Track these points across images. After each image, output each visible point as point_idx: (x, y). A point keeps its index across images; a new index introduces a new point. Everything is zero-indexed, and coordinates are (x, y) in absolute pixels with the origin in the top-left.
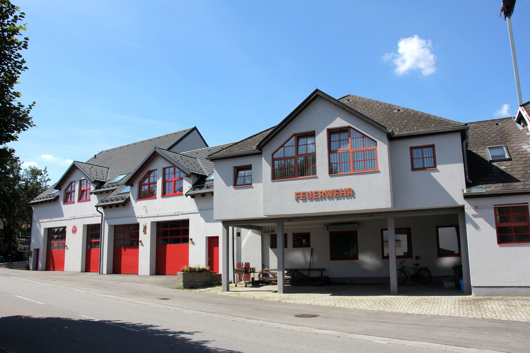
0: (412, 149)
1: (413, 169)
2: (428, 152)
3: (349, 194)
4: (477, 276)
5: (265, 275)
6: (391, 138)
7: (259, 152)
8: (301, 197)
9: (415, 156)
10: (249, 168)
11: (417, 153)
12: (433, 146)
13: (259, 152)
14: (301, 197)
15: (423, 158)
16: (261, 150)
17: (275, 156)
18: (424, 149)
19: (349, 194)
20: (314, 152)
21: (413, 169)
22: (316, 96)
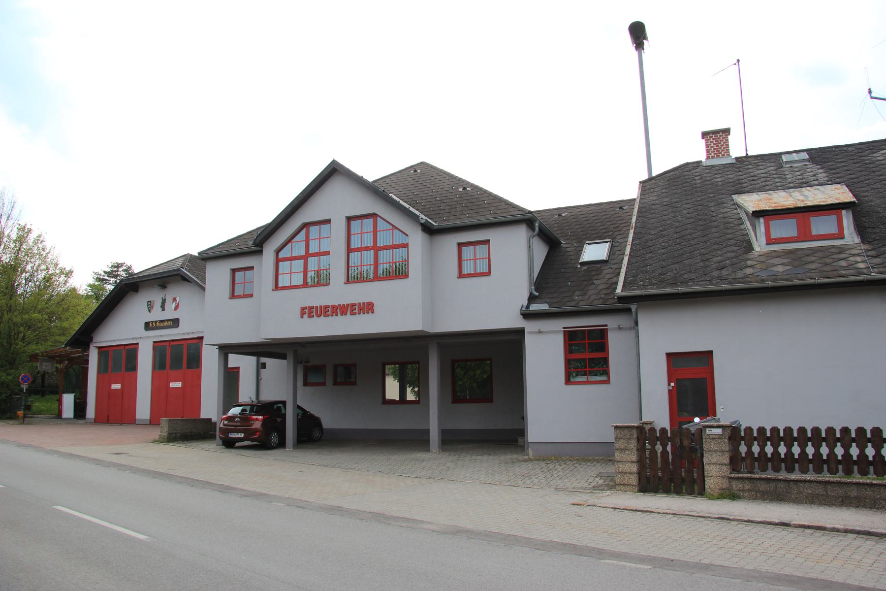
0: (460, 245)
1: (461, 275)
2: (481, 250)
3: (368, 308)
4: (537, 429)
5: (319, 280)
6: (429, 230)
7: (258, 248)
8: (308, 312)
9: (464, 257)
10: (252, 268)
11: (467, 252)
12: (487, 242)
13: (258, 248)
14: (308, 312)
15: (475, 259)
16: (262, 247)
17: (281, 255)
18: (477, 247)
19: (368, 308)
20: (635, 432)
21: (461, 275)
22: (334, 171)
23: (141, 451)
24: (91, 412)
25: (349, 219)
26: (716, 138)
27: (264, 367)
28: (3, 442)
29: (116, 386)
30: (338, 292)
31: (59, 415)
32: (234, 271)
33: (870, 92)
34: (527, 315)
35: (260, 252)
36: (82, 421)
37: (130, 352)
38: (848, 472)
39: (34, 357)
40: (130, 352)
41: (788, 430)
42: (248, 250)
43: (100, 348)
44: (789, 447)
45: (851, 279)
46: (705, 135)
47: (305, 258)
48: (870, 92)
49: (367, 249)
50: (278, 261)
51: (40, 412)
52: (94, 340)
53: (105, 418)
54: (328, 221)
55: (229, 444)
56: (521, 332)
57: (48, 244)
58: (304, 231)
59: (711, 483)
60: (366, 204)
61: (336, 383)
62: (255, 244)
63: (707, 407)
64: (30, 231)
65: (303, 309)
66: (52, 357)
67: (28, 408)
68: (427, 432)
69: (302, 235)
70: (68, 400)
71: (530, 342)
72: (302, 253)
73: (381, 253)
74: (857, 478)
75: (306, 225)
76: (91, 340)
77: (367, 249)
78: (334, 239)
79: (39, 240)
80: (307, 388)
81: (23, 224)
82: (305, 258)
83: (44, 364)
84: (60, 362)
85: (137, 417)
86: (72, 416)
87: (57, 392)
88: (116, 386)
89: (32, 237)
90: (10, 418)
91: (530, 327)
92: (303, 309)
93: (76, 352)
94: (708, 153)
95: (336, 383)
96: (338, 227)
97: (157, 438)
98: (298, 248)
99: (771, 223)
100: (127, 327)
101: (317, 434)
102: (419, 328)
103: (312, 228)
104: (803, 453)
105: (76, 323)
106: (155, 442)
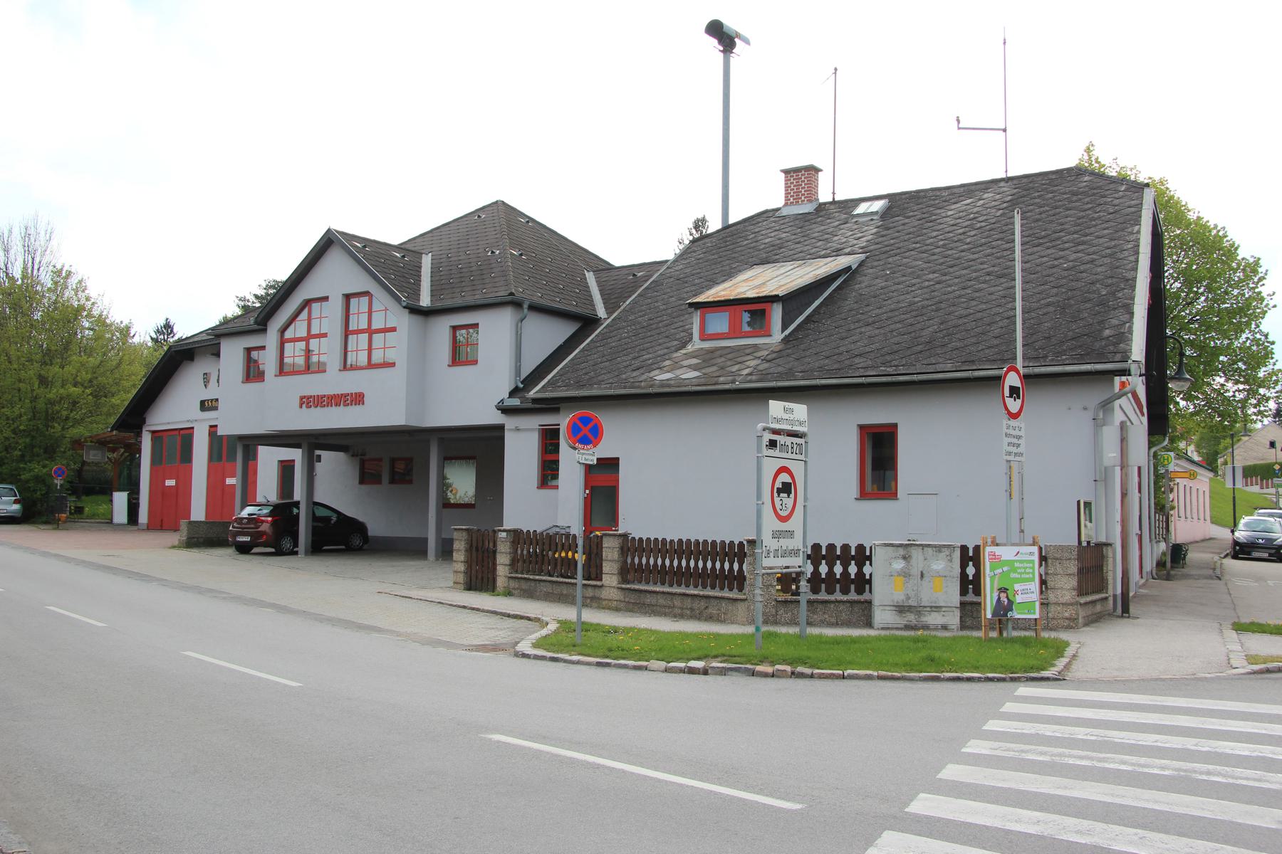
3: (358, 399)
8: (308, 401)
14: (308, 401)
17: (288, 334)
19: (358, 399)
22: (328, 242)
23: (158, 554)
24: (143, 517)
25: (348, 297)
26: (801, 178)
27: (319, 461)
28: (1, 544)
29: (170, 483)
30: (333, 382)
31: (110, 521)
32: (249, 350)
33: (958, 121)
34: (506, 411)
35: (264, 330)
36: (135, 528)
37: (185, 436)
38: (830, 591)
39: (77, 444)
40: (185, 436)
41: (831, 547)
42: (247, 328)
43: (153, 432)
44: (845, 566)
45: (727, 387)
46: (786, 172)
47: (307, 339)
48: (958, 121)
49: (362, 331)
50: (282, 342)
51: (93, 516)
52: (148, 422)
53: (160, 523)
54: (326, 299)
55: (244, 549)
56: (500, 428)
57: (93, 291)
58: (306, 311)
59: (501, 582)
60: (360, 281)
61: (392, 481)
62: (256, 323)
63: (613, 518)
64: (69, 274)
65: (302, 398)
66: (102, 443)
67: (79, 510)
68: (425, 540)
69: (304, 315)
70: (120, 499)
71: (509, 438)
72: (304, 334)
73: (375, 336)
74: (838, 596)
75: (307, 303)
76: (143, 422)
77: (362, 331)
78: (328, 319)
79: (81, 287)
80: (364, 487)
81: (59, 267)
82: (307, 339)
83: (92, 452)
84: (113, 450)
85: (370, 534)
86: (125, 520)
87: (105, 490)
88: (170, 483)
89: (73, 282)
90: (46, 523)
91: (510, 422)
92: (302, 398)
93: (128, 436)
94: (787, 199)
95: (392, 481)
96: (336, 305)
97: (176, 543)
98: (299, 329)
99: (708, 316)
100: (177, 409)
101: (357, 541)
102: (403, 423)
103: (314, 305)
104: (831, 572)
105: (123, 399)
106: (174, 547)
